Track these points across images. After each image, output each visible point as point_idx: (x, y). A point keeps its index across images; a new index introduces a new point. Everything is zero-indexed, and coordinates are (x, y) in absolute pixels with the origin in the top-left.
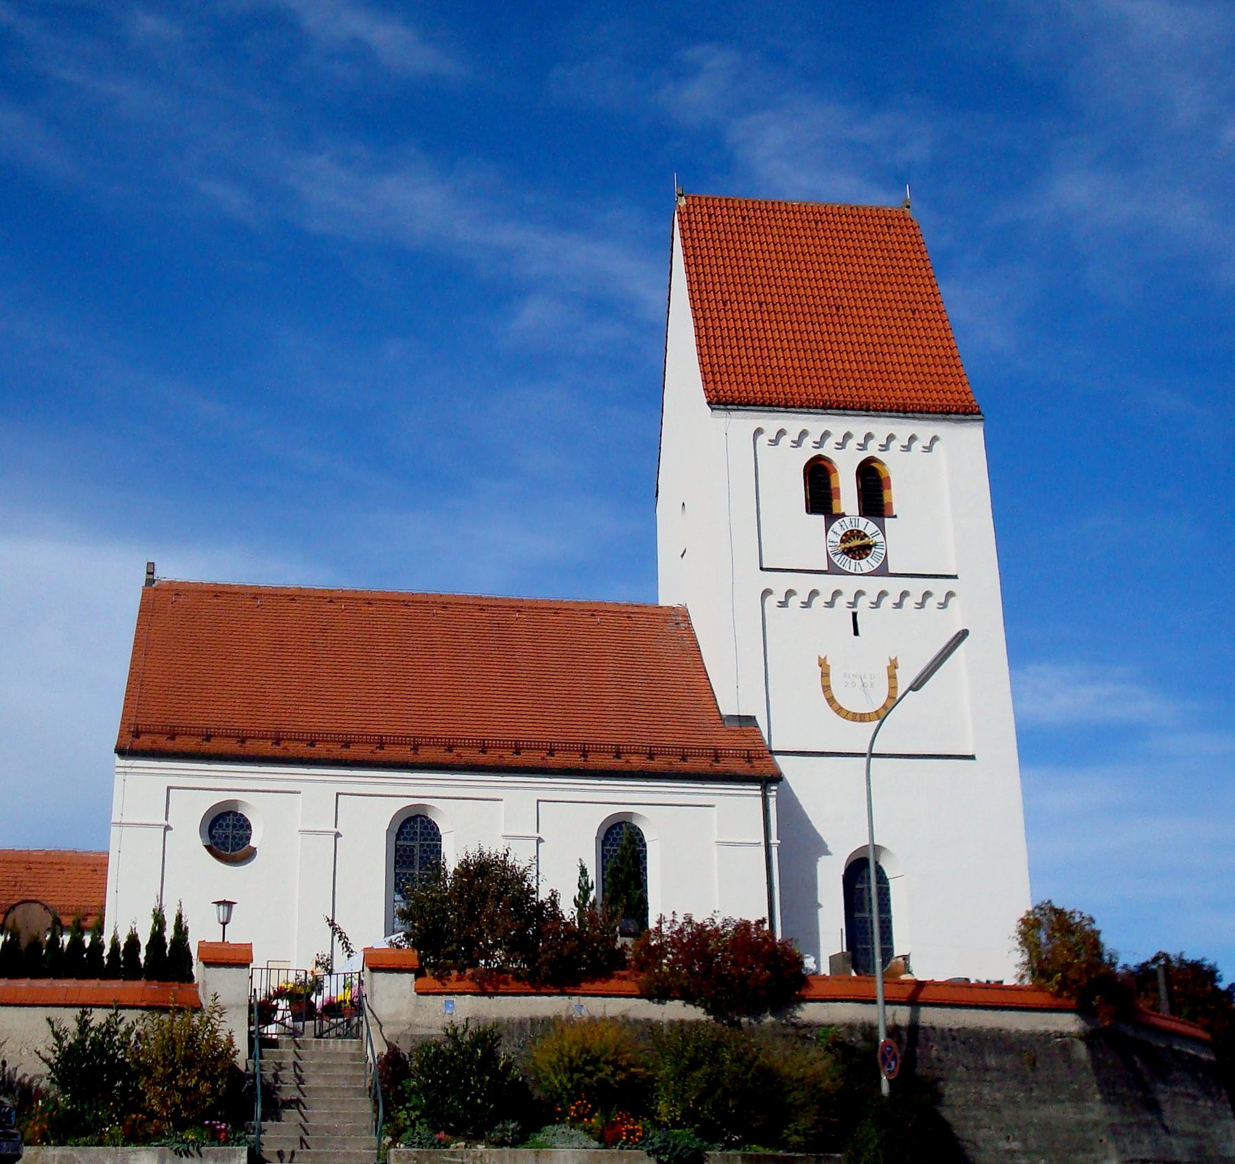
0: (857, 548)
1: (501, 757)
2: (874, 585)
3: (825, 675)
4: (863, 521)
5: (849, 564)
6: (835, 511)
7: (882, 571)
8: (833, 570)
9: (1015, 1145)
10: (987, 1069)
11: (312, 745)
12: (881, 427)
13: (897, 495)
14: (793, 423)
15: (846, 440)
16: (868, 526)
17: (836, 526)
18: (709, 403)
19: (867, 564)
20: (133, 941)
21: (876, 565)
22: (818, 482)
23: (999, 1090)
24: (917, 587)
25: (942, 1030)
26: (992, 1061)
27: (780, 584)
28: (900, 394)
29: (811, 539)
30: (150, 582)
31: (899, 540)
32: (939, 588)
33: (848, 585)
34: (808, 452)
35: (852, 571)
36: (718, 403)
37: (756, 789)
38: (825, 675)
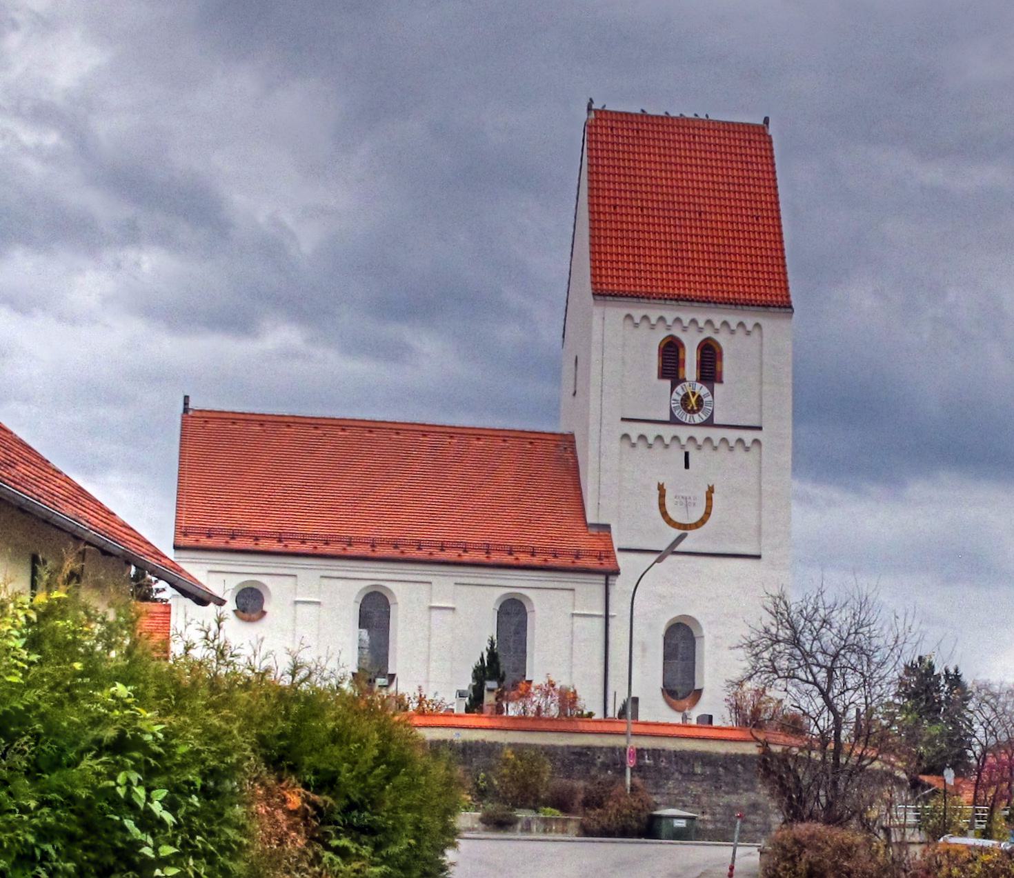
0: (691, 404)
1: (431, 554)
2: (700, 434)
3: (662, 496)
4: (698, 385)
5: (686, 418)
6: (681, 377)
7: (709, 423)
8: (674, 421)
9: (707, 817)
10: (695, 774)
11: (303, 542)
12: (718, 317)
13: (728, 366)
14: (654, 315)
15: (692, 326)
16: (702, 390)
17: (679, 389)
18: (594, 294)
19: (697, 418)
20: (174, 823)
21: (705, 418)
22: (671, 353)
23: (700, 786)
24: (732, 435)
25: (670, 752)
26: (698, 770)
27: (635, 430)
28: (500, 627)
29: (660, 398)
30: (186, 410)
31: (725, 401)
32: (748, 436)
33: (683, 433)
34: (661, 335)
35: (687, 421)
36: (599, 295)
37: (602, 578)
38: (662, 496)
